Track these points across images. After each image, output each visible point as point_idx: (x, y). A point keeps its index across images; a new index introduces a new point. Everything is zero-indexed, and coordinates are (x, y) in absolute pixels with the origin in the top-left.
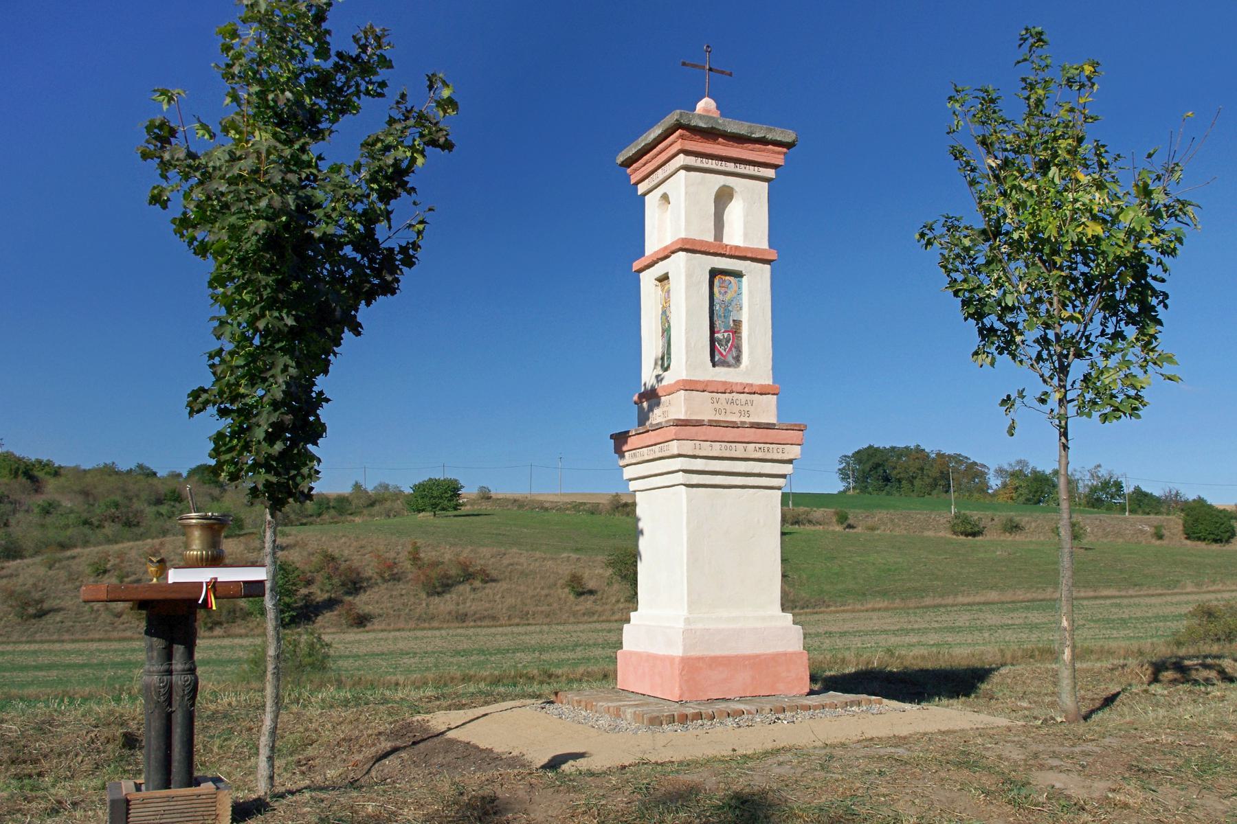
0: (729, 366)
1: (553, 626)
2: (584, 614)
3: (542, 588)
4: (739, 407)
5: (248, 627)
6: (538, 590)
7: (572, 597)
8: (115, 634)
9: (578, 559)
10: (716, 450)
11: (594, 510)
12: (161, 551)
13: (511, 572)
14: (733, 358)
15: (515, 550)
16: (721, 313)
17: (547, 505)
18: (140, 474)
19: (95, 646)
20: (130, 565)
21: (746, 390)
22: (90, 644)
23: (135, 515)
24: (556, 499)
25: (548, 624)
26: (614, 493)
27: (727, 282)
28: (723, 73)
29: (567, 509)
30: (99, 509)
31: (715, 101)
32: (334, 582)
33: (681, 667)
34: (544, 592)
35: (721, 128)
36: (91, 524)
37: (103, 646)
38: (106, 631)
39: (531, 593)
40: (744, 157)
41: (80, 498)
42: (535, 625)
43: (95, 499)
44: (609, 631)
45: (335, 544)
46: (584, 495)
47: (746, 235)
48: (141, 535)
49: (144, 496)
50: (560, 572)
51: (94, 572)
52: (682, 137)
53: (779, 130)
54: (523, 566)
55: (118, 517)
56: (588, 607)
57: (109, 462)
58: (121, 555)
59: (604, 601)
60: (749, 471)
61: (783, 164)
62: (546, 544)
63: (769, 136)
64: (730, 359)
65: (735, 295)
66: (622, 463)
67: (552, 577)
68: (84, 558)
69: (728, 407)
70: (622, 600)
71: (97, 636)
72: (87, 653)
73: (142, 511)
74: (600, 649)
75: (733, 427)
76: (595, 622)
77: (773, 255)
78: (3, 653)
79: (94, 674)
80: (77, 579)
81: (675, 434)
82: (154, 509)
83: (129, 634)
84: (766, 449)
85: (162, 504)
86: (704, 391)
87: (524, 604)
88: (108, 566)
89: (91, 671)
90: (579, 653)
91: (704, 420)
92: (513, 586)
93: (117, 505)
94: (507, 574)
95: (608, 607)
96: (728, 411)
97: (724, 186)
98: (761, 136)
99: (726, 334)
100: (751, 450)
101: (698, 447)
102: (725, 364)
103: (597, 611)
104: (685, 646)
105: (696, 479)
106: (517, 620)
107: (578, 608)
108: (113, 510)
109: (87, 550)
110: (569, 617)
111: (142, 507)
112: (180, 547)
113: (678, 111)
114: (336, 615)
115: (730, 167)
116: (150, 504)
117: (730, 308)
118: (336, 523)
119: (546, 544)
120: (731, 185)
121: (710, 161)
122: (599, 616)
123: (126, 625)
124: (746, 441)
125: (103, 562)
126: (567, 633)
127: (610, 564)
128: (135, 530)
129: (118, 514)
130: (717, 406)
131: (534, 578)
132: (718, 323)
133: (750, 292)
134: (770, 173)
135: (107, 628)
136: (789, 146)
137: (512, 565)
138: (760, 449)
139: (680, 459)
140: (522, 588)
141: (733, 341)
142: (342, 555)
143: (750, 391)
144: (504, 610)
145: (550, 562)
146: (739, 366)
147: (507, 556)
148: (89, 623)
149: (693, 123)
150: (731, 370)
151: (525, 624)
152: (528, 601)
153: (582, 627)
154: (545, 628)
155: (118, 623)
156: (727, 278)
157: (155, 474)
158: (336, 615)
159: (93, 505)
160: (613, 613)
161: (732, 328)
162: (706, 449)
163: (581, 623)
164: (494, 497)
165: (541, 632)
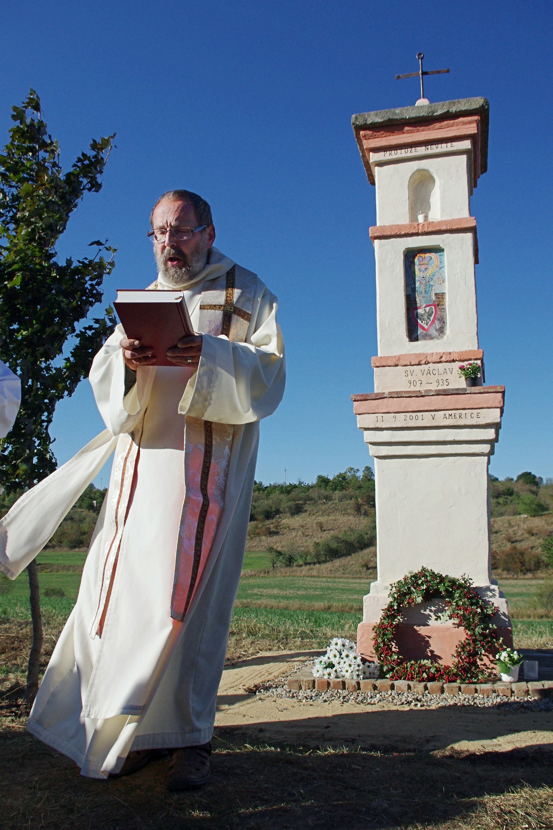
0: (432, 338)
4: (437, 377)
5: (547, 573)
10: (400, 420)
12: (495, 526)
14: (436, 330)
21: (443, 359)
35: (398, 118)
53: (463, 101)
63: (453, 109)
64: (433, 332)
65: (437, 269)
69: (424, 379)
77: (472, 223)
82: (495, 500)
84: (458, 416)
86: (396, 365)
91: (384, 393)
97: (418, 171)
98: (443, 112)
100: (440, 419)
101: (380, 419)
115: (421, 151)
117: (431, 283)
120: (426, 168)
124: (432, 408)
130: (410, 378)
134: (467, 144)
138: (450, 415)
141: (436, 314)
143: (448, 359)
146: (442, 337)
149: (369, 121)
150: (436, 341)
156: (428, 255)
157: (497, 479)
161: (434, 301)
162: (389, 421)
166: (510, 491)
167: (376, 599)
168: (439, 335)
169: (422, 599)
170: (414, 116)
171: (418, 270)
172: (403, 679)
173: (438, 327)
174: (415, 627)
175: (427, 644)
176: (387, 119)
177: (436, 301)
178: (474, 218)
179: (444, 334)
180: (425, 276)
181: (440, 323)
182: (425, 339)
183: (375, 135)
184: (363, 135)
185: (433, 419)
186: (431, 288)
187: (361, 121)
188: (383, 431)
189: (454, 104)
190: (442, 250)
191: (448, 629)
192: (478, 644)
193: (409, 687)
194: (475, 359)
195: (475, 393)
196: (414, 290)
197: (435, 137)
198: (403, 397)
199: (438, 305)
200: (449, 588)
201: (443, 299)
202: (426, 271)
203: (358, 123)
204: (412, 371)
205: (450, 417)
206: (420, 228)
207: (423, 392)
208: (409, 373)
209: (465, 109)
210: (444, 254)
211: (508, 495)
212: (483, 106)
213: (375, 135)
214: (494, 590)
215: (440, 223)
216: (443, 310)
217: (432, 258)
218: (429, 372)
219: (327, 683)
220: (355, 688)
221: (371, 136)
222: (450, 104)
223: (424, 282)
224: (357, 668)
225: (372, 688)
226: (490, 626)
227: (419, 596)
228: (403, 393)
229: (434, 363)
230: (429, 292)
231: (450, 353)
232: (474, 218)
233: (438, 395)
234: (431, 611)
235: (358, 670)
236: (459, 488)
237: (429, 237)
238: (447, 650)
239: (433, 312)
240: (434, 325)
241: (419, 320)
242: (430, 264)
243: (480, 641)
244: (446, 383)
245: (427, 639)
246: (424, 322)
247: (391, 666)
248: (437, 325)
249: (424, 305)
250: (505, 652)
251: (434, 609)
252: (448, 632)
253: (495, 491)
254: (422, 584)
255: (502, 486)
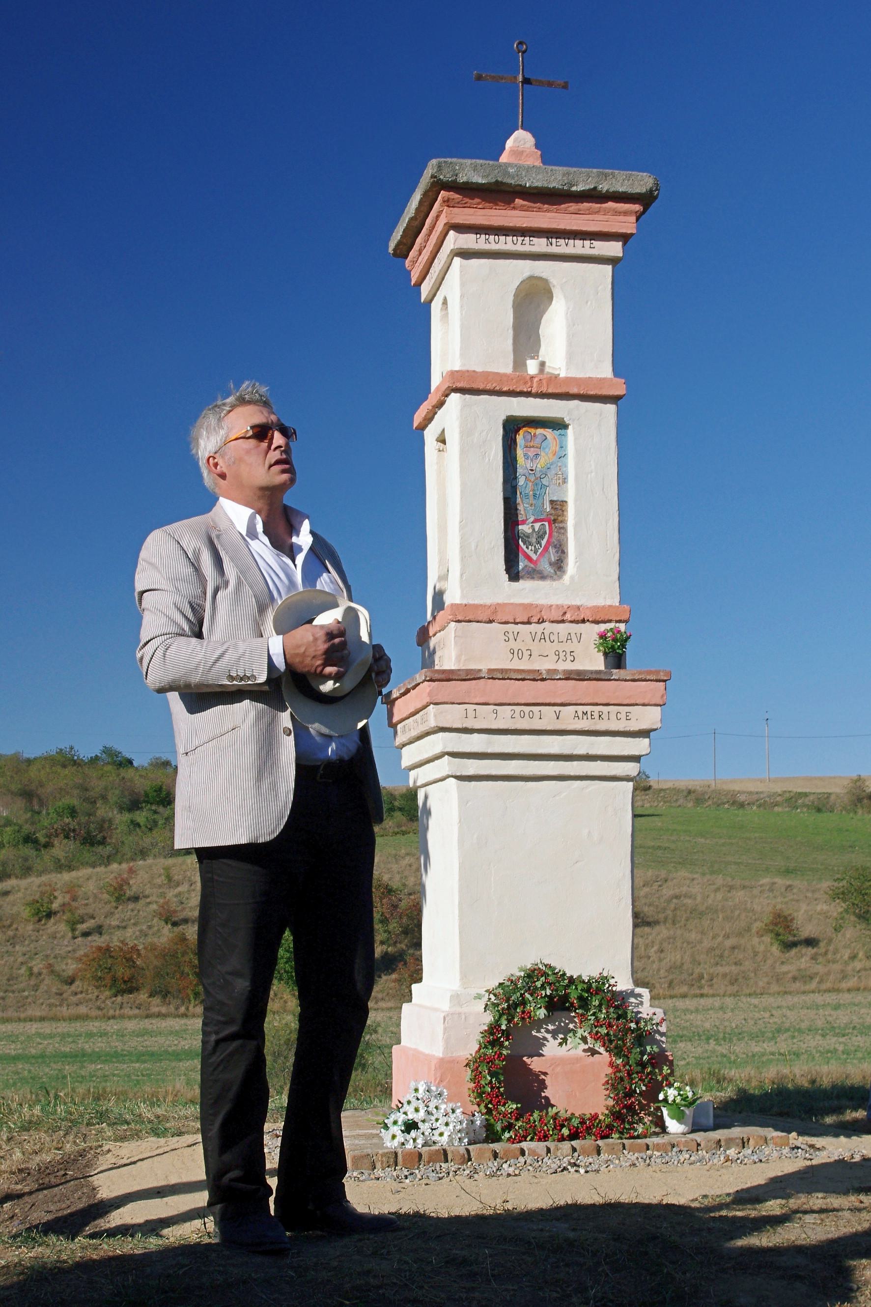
0: (543, 577)
1: (744, 999)
2: (795, 979)
3: (726, 936)
4: (556, 646)
6: (720, 939)
7: (775, 949)
8: (64, 1011)
9: (789, 888)
10: (505, 718)
11: (822, 805)
13: (675, 909)
14: (551, 564)
15: (683, 873)
16: (529, 490)
17: (742, 798)
18: (108, 763)
19: (33, 1028)
20: (87, 905)
21: (568, 617)
22: (28, 1025)
23: (101, 829)
24: (760, 787)
25: (735, 995)
26: (854, 775)
27: (538, 440)
28: (550, 84)
29: (777, 804)
30: (48, 820)
31: (534, 136)
32: (391, 927)
33: (439, 1075)
34: (729, 943)
35: (513, 182)
36: (36, 841)
37: (47, 1028)
38: (50, 1005)
39: (707, 944)
40: (562, 226)
41: (20, 803)
42: (713, 996)
43: (42, 803)
44: (837, 1007)
45: (395, 867)
46: (810, 779)
47: (570, 357)
48: (109, 857)
49: (113, 797)
50: (757, 908)
51: (33, 915)
52: (447, 202)
53: (621, 174)
54: (695, 899)
55: (74, 830)
56: (803, 966)
57: (64, 745)
58: (72, 890)
59: (830, 956)
60: (566, 751)
61: (634, 231)
62: (735, 863)
63: (604, 187)
64: (545, 566)
65: (555, 459)
66: (400, 739)
67: (743, 916)
68: (20, 895)
69: (536, 647)
70: (861, 955)
71: (38, 1014)
72: (22, 1038)
73: (110, 821)
74: (818, 1037)
75: (534, 680)
76: (813, 992)
77: (619, 388)
78: (865, 1030)
79: (30, 1071)
80: (10, 926)
81: (429, 694)
82: (127, 816)
83: (83, 1010)
84: (596, 715)
85: (139, 808)
86: (491, 622)
87: (696, 962)
88: (55, 906)
89: (27, 1066)
90: (783, 1045)
91: (480, 670)
92: (679, 932)
93: (73, 812)
94: (669, 912)
95: (836, 967)
96: (535, 654)
97: (531, 278)
98: (587, 187)
99: (537, 526)
100: (568, 718)
101: (471, 713)
102: (536, 574)
103: (817, 974)
104: (447, 1041)
105: (473, 767)
106: (684, 989)
107: (785, 968)
108: (67, 820)
109: (23, 883)
110: (768, 983)
111: (110, 814)
112: (160, 875)
113: (434, 162)
114: (395, 981)
115: (540, 245)
116: (121, 809)
118: (404, 833)
119: (735, 863)
120: (544, 275)
121: (502, 238)
122: (821, 982)
123: (79, 996)
124: (559, 701)
125: (46, 900)
126: (765, 1009)
127: (839, 895)
128: (100, 849)
129: (73, 824)
130: (512, 644)
131: (713, 920)
132: (523, 508)
133: (577, 451)
134: (614, 249)
135: (52, 1001)
136: (646, 200)
137: (677, 897)
138: (585, 713)
139: (441, 734)
140: (693, 936)
142: (404, 885)
144: (662, 972)
145: (741, 893)
146: (560, 577)
147: (670, 883)
148: (26, 993)
149: (462, 179)
151: (696, 996)
152: (702, 957)
153: (790, 1000)
154: (729, 1001)
155: (69, 991)
156: (540, 431)
157: (130, 762)
158: (395, 981)
159: (39, 813)
160: (844, 977)
162: (486, 717)
163: (790, 993)
164: (655, 786)
165: (721, 1008)
166: (164, 794)
167: (463, 1017)
168: (556, 574)
169: (546, 1012)
170: (539, 184)
171: (522, 455)
172: (530, 1140)
173: (553, 560)
174: (525, 1059)
175: (543, 1085)
176: (494, 180)
177: (551, 514)
178: (623, 381)
179: (564, 572)
180: (534, 468)
181: (557, 552)
182: (533, 578)
183: (466, 203)
184: (446, 199)
185: (558, 718)
186: (543, 490)
187: (448, 176)
188: (471, 733)
189: (606, 177)
190: (565, 426)
191: (578, 1060)
192: (635, 1078)
193: (548, 1150)
194: (617, 622)
195: (626, 680)
196: (514, 489)
197: (568, 228)
198: (511, 679)
199: (555, 521)
200: (583, 994)
201: (563, 511)
202: (536, 459)
203: (441, 177)
204: (516, 634)
205: (585, 717)
206: (535, 385)
207: (544, 672)
208: (511, 636)
209: (624, 190)
210: (566, 433)
211: (158, 803)
212: (651, 191)
213: (466, 203)
214: (640, 995)
215: (569, 380)
216: (562, 531)
217: (546, 438)
218: (543, 637)
219: (417, 1154)
220: (464, 1158)
221: (458, 203)
222: (598, 176)
223: (532, 478)
224: (459, 1127)
225: (492, 1157)
226: (648, 1048)
227: (540, 1008)
228: (512, 673)
229: (553, 622)
230: (541, 498)
231: (578, 608)
232: (623, 381)
233: (567, 679)
234: (548, 1031)
235: (459, 1131)
236: (589, 832)
237: (545, 401)
238: (578, 1094)
239: (546, 533)
240: (546, 555)
241: (521, 543)
242: (544, 449)
243: (637, 1073)
244: (570, 658)
245: (543, 1077)
246: (530, 547)
247: (508, 1122)
248: (553, 555)
249: (532, 519)
250: (672, 1089)
251: (553, 1027)
252: (578, 1065)
253: (126, 793)
254: (543, 987)
255: (142, 780)
